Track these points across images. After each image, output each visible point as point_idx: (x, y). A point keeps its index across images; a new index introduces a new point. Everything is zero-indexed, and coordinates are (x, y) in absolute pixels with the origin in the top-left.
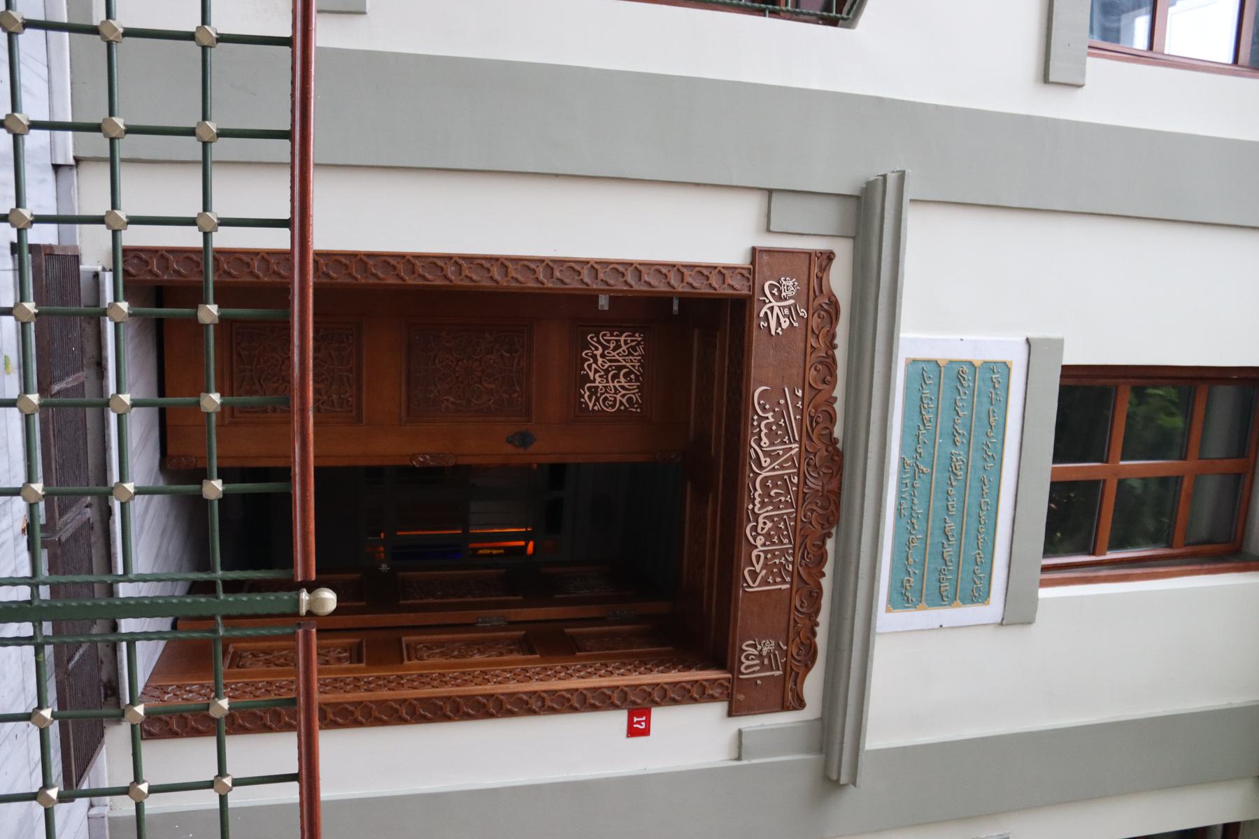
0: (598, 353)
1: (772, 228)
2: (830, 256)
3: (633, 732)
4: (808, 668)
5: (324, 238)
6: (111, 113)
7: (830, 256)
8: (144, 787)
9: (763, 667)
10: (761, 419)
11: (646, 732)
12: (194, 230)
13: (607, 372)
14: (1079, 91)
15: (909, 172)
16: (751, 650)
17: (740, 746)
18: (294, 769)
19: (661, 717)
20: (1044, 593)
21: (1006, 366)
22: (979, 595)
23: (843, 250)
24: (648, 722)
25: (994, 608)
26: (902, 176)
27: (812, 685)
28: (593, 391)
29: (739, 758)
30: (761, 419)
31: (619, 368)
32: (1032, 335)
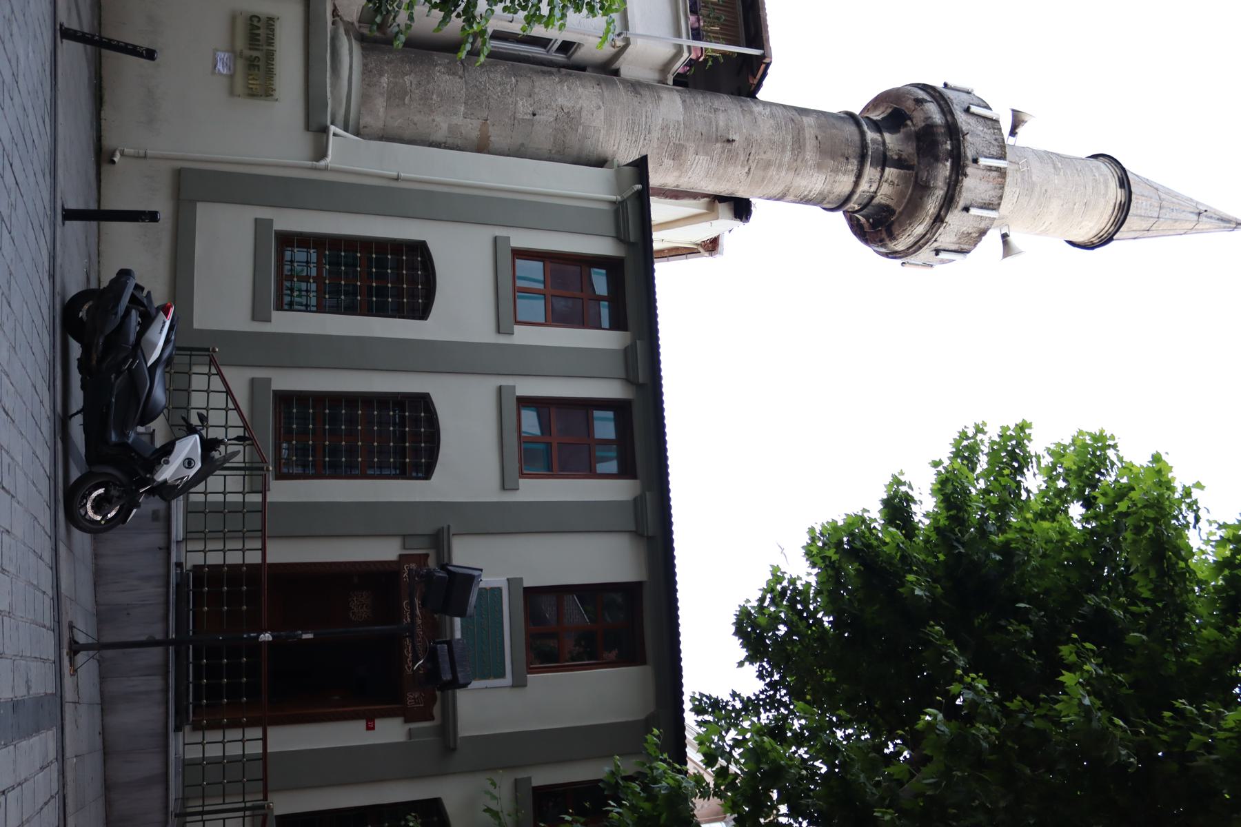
0: (355, 599)
1: (406, 547)
2: (427, 556)
3: (369, 728)
4: (434, 703)
5: (269, 560)
6: (224, 528)
7: (427, 556)
8: (245, 510)
9: (416, 703)
10: (407, 612)
11: (373, 728)
12: (241, 533)
13: (359, 606)
14: (518, 492)
15: (451, 525)
16: (410, 696)
17: (410, 733)
18: (261, 737)
19: (379, 723)
20: (528, 676)
21: (499, 590)
22: (502, 675)
23: (432, 553)
24: (374, 724)
25: (508, 680)
26: (449, 527)
27: (437, 710)
28: (353, 613)
29: (410, 739)
30: (407, 612)
31: (363, 605)
32: (509, 577)
